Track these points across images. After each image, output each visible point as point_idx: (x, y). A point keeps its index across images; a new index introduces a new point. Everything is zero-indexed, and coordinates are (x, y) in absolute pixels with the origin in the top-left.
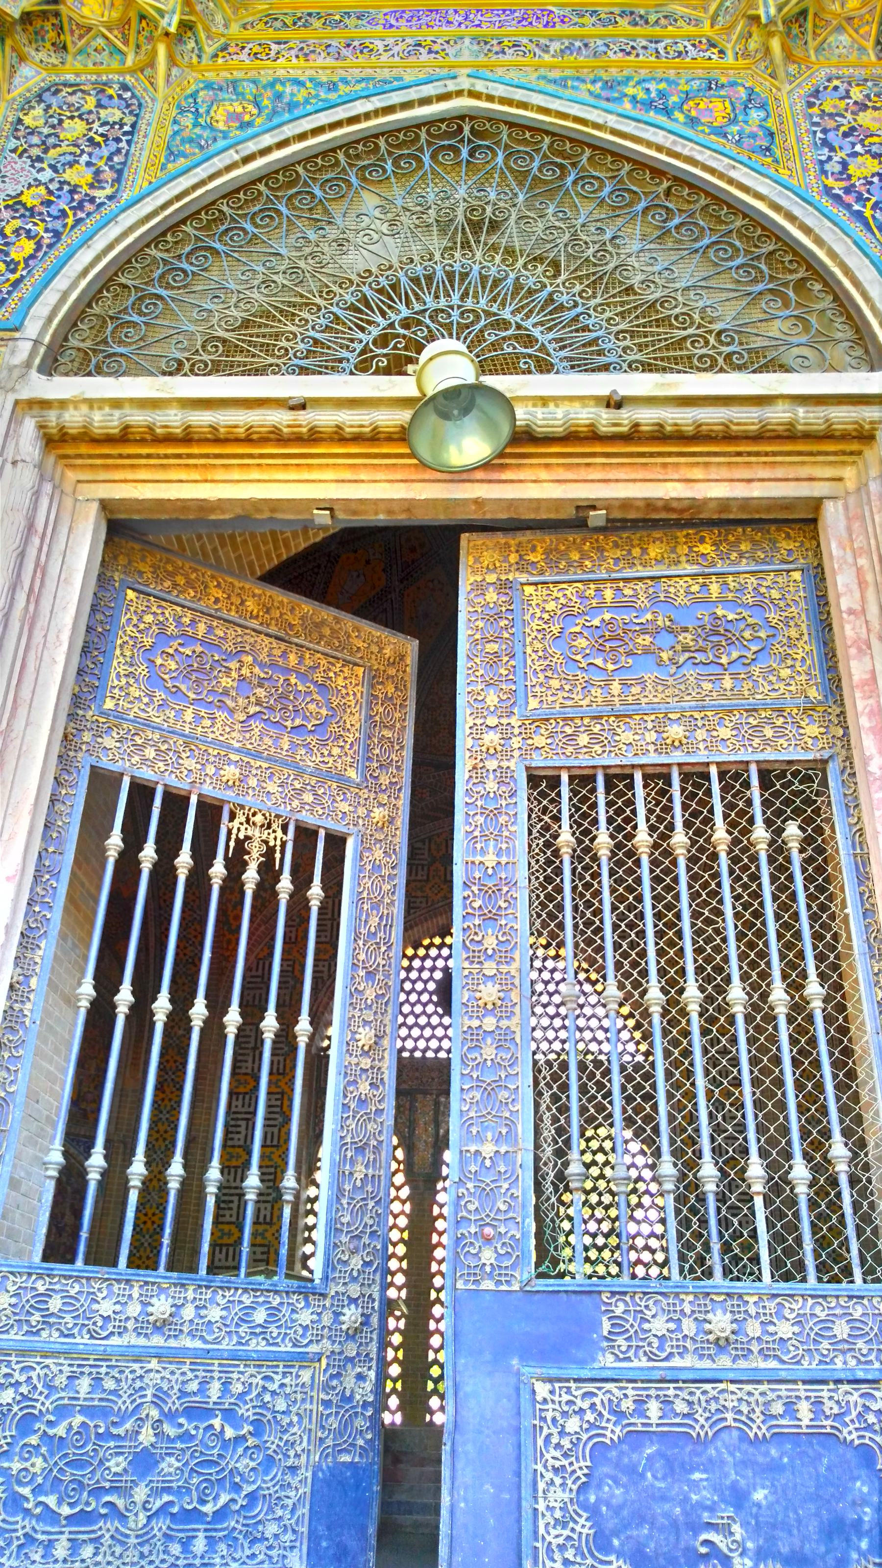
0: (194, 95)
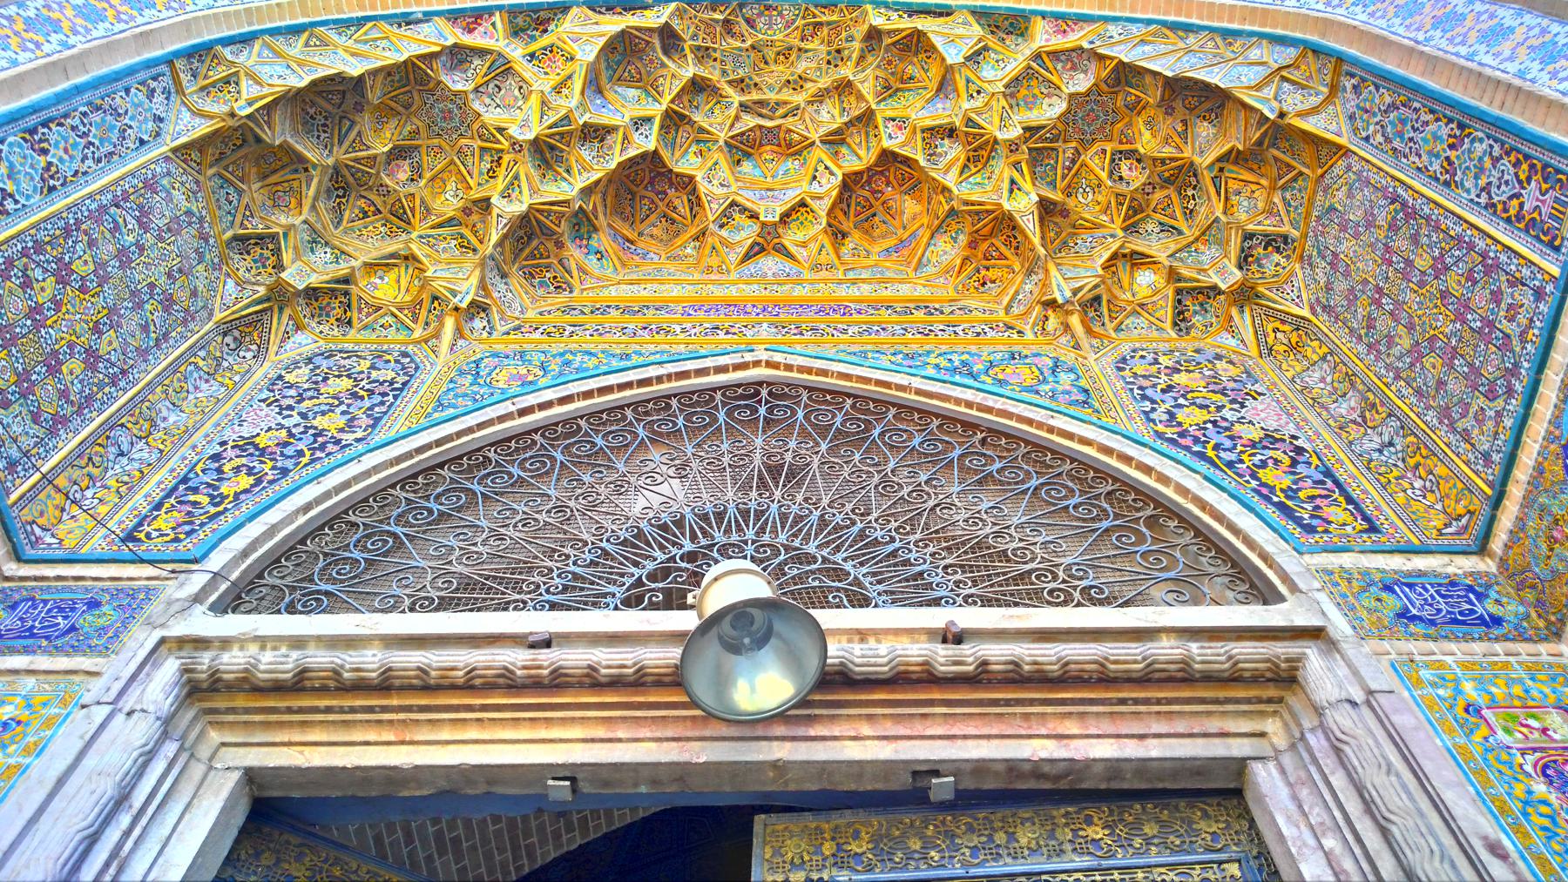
0: (477, 363)
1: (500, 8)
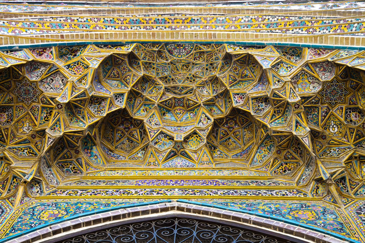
0: (33, 209)
1: (55, 45)
